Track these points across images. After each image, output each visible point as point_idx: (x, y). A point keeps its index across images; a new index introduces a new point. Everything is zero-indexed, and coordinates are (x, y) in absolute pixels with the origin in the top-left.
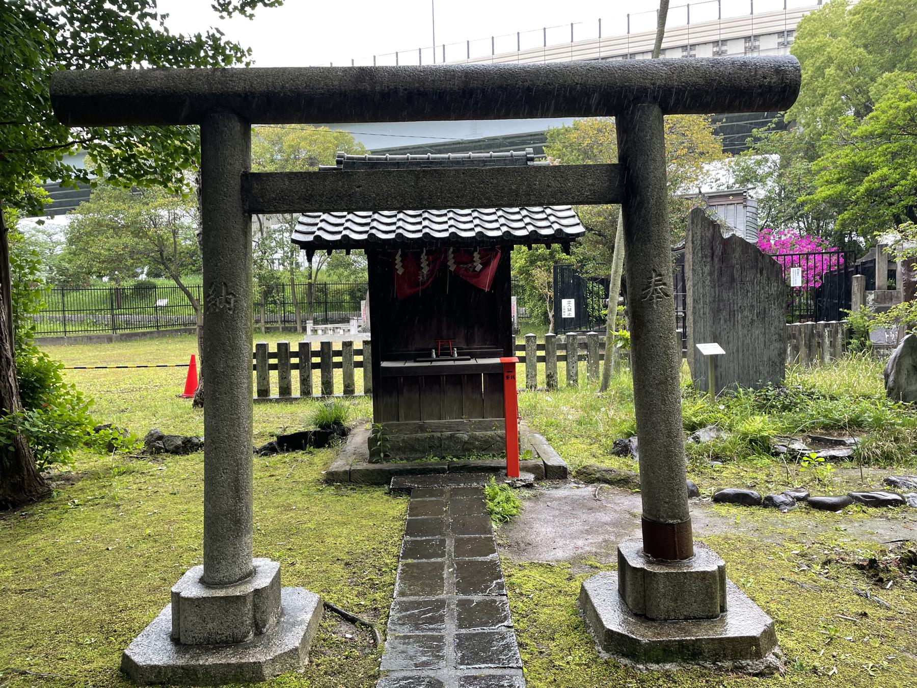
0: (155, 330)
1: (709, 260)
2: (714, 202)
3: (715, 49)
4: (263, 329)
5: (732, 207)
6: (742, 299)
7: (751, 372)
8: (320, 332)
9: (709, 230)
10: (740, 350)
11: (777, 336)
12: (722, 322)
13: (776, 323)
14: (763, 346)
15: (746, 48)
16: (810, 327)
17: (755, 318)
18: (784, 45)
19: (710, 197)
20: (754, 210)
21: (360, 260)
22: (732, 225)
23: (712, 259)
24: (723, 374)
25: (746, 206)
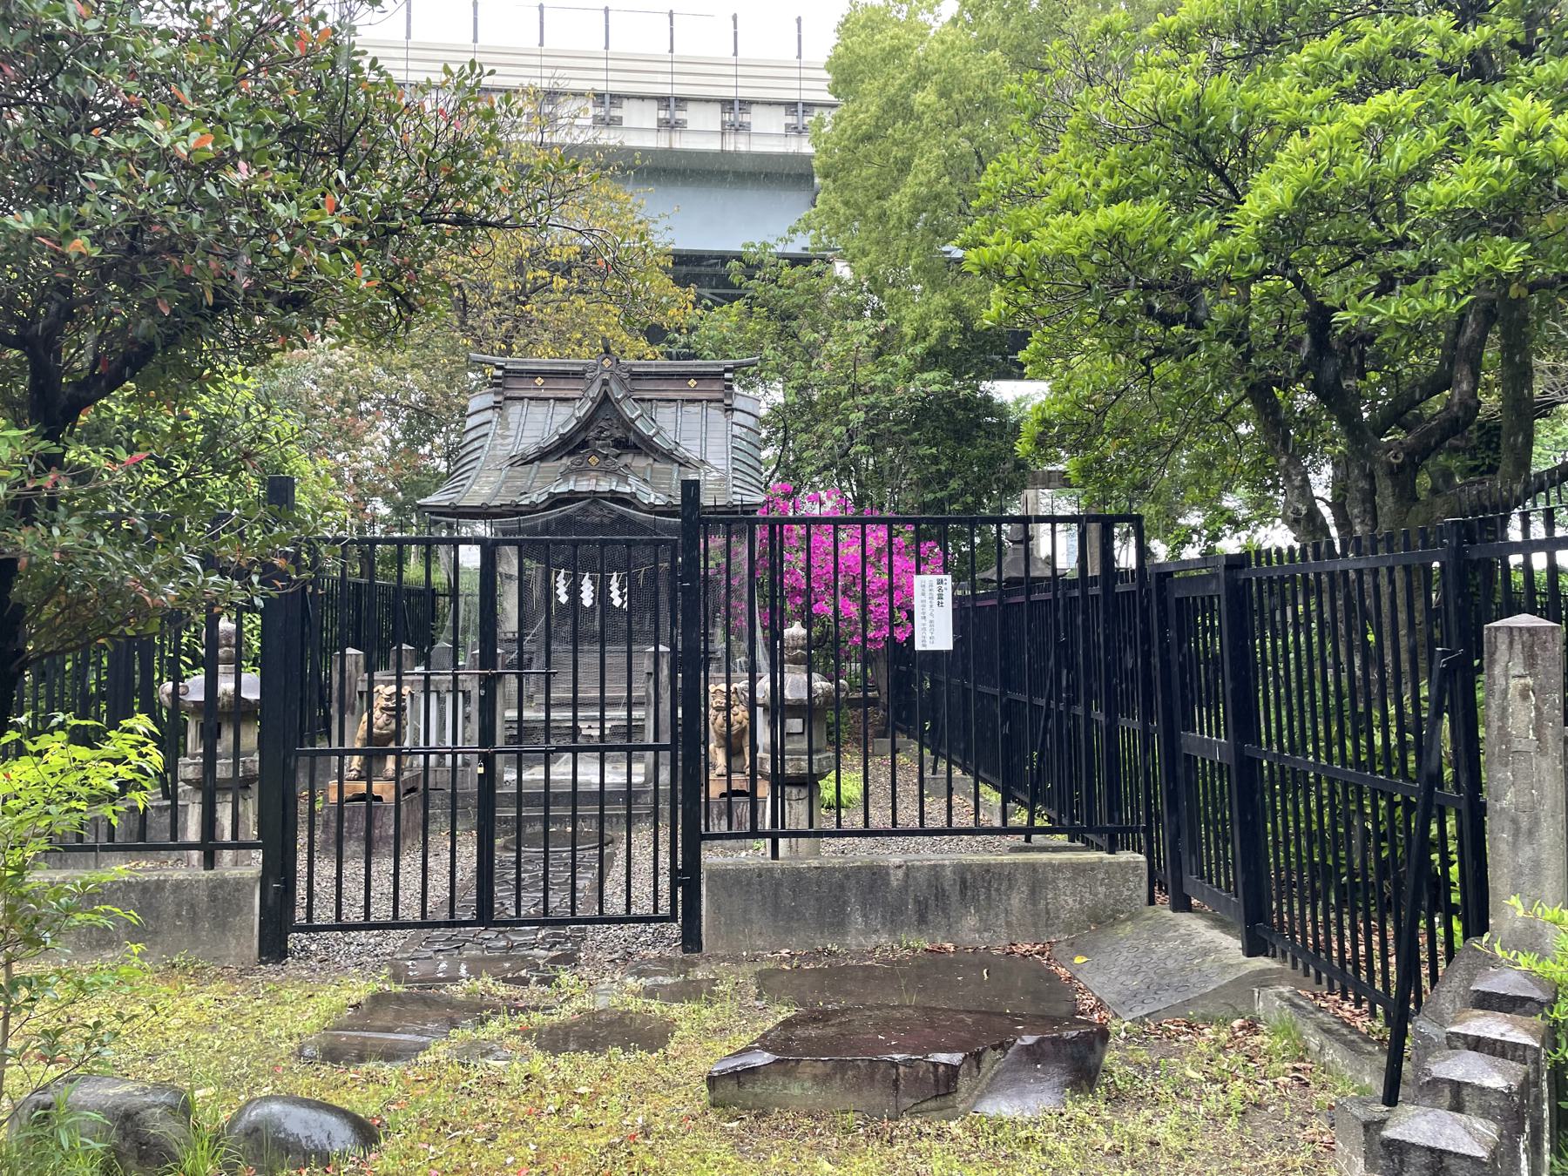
2: (648, 390)
3: (662, 114)
15: (723, 123)
18: (798, 130)
21: (926, 546)
22: (694, 455)
25: (729, 409)
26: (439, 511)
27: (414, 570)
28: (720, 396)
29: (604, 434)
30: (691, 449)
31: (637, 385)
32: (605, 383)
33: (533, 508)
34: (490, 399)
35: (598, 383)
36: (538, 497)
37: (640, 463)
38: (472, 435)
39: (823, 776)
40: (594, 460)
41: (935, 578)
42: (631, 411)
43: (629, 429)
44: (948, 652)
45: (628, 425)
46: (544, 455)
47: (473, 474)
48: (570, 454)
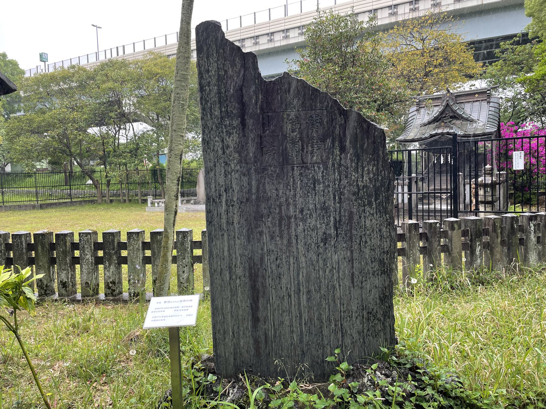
0: (69, 200)
1: (236, 122)
4: (140, 200)
5: (478, 103)
6: (306, 196)
7: (326, 332)
8: (156, 204)
9: (233, 65)
10: (303, 289)
11: (376, 266)
12: (266, 238)
13: (375, 241)
14: (348, 283)
16: (509, 221)
17: (332, 231)
19: (457, 96)
20: (496, 105)
23: (243, 123)
24: (271, 333)
25: (489, 102)
26: (401, 141)
27: (395, 156)
28: (486, 98)
29: (448, 115)
30: (474, 116)
31: (458, 99)
32: (448, 101)
33: (426, 138)
34: (415, 108)
35: (446, 101)
36: (427, 135)
37: (458, 122)
38: (410, 119)
39: (495, 202)
40: (443, 124)
41: (519, 152)
42: (455, 108)
43: (455, 113)
44: (522, 170)
45: (454, 112)
46: (429, 123)
47: (410, 130)
48: (437, 122)
